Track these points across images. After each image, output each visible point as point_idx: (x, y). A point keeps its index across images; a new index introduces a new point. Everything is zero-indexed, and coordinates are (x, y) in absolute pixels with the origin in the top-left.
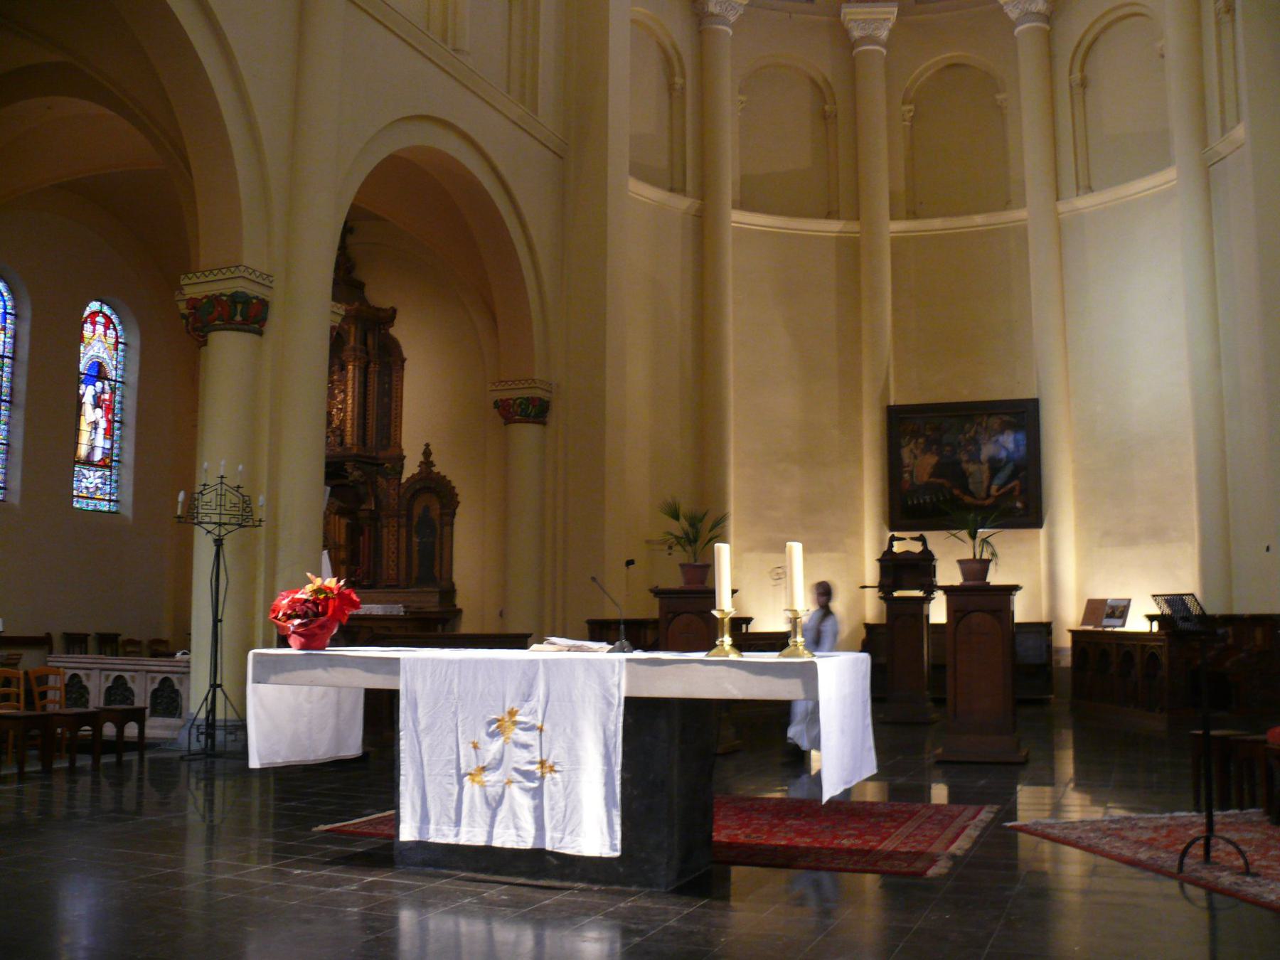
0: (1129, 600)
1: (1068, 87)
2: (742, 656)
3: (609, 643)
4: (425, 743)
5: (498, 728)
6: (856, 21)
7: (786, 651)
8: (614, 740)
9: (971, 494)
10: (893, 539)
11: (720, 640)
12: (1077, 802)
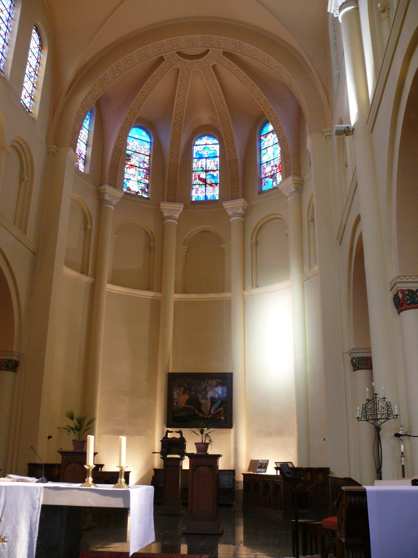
1: (250, 244)
2: (97, 487)
3: (37, 478)
6: (166, 209)
7: (117, 485)
8: (35, 526)
9: (202, 413)
10: (168, 432)
11: (87, 479)
12: (244, 553)
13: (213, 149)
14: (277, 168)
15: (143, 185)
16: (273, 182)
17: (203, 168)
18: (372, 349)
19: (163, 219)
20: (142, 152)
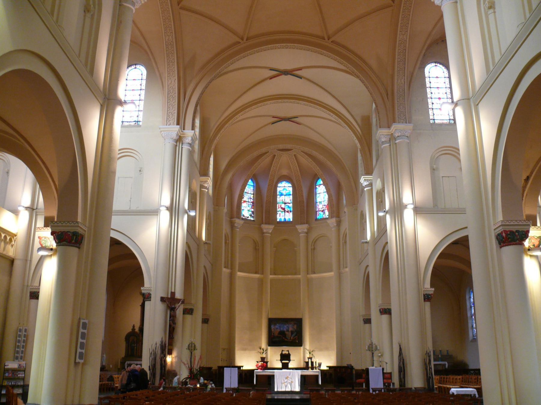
0: (321, 363)
4: (278, 380)
5: (287, 378)
9: (287, 339)
13: (289, 190)
14: (326, 207)
15: (251, 212)
16: (323, 214)
17: (283, 201)
18: (372, 315)
19: (263, 233)
20: (249, 192)
